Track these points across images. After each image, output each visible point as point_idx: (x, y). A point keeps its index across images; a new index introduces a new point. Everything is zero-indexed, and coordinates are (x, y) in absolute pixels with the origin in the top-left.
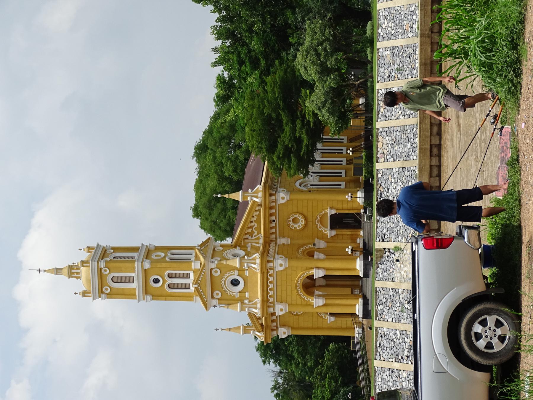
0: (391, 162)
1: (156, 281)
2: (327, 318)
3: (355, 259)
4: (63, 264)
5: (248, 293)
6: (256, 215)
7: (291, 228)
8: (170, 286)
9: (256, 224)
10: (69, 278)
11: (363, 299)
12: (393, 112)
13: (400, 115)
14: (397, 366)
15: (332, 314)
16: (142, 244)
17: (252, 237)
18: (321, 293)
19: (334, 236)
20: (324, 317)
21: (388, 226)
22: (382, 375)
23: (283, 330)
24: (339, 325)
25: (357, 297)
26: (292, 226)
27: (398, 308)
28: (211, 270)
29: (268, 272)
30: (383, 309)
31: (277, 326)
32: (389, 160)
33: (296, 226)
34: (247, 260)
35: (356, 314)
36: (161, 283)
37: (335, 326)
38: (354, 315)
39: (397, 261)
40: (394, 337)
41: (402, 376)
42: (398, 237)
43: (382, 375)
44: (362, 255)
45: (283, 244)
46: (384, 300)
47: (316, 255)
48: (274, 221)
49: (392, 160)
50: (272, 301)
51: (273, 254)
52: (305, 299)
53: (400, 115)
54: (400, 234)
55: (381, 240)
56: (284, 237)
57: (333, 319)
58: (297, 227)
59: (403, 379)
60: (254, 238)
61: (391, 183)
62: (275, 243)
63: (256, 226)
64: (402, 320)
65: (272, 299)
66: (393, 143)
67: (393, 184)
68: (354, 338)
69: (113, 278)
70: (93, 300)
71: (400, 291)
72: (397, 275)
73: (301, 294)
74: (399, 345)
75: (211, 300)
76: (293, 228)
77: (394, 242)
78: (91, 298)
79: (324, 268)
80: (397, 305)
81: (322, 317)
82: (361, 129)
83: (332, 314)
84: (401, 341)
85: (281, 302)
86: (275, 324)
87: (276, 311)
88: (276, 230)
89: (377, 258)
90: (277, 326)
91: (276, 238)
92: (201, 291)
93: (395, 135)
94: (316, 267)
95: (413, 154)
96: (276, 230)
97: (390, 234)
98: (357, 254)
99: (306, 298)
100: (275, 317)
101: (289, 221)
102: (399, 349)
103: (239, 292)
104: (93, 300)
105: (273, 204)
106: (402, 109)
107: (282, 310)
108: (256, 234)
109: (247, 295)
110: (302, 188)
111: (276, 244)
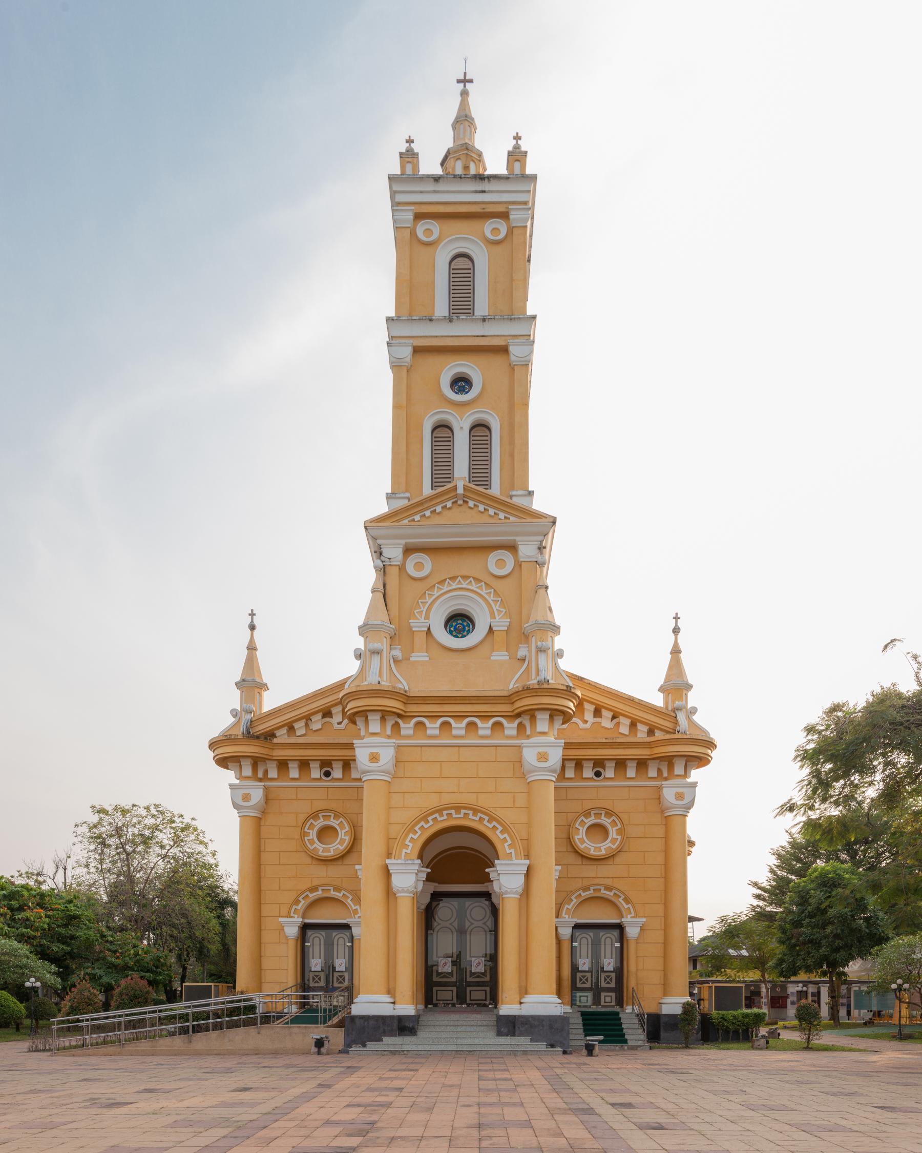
2: (292, 914)
9: (588, 726)
20: (294, 907)
28: (512, 548)
31: (265, 778)
33: (583, 831)
37: (267, 937)
48: (327, 774)
50: (403, 732)
52: (411, 835)
57: (292, 931)
63: (582, 725)
75: (403, 542)
76: (577, 826)
79: (526, 891)
82: (900, 1023)
85: (398, 762)
86: (273, 774)
89: (136, 1033)
92: (439, 509)
99: (415, 837)
101: (598, 815)
107: (374, 758)
109: (420, 656)
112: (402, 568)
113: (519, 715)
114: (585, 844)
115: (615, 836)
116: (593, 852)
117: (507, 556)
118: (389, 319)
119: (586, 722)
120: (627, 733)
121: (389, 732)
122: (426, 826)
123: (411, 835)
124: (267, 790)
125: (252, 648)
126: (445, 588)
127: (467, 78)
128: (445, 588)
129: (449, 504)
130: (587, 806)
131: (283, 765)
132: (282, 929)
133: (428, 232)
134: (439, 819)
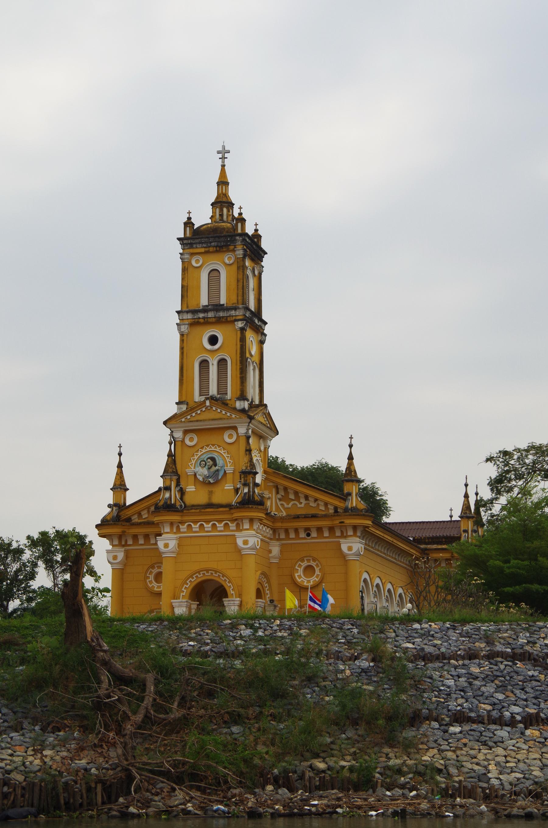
1: (213, 340)
4: (233, 194)
5: (194, 490)
6: (318, 505)
7: (296, 563)
8: (204, 364)
17: (280, 500)
26: (300, 566)
28: (235, 428)
29: (233, 520)
31: (126, 545)
33: (300, 571)
34: (275, 497)
36: (208, 347)
45: (270, 551)
48: (308, 535)
50: (181, 530)
52: (185, 586)
56: (281, 552)
58: (299, 574)
60: (279, 503)
62: (272, 537)
63: (299, 506)
65: (185, 530)
69: (216, 272)
73: (187, 584)
75: (183, 429)
76: (296, 568)
78: (182, 236)
85: (179, 545)
86: (130, 542)
88: (293, 539)
91: (279, 539)
92: (199, 412)
94: (241, 602)
96: (293, 539)
99: (187, 586)
101: (308, 561)
105: (338, 533)
107: (166, 546)
108: (286, 506)
111: (271, 539)
112: (183, 441)
113: (236, 520)
114: (311, 581)
115: (318, 573)
118: (178, 312)
119: (301, 503)
120: (324, 509)
121: (175, 531)
122: (193, 580)
123: (185, 586)
125: (120, 466)
128: (204, 451)
129: (204, 409)
131: (135, 537)
134: (199, 576)
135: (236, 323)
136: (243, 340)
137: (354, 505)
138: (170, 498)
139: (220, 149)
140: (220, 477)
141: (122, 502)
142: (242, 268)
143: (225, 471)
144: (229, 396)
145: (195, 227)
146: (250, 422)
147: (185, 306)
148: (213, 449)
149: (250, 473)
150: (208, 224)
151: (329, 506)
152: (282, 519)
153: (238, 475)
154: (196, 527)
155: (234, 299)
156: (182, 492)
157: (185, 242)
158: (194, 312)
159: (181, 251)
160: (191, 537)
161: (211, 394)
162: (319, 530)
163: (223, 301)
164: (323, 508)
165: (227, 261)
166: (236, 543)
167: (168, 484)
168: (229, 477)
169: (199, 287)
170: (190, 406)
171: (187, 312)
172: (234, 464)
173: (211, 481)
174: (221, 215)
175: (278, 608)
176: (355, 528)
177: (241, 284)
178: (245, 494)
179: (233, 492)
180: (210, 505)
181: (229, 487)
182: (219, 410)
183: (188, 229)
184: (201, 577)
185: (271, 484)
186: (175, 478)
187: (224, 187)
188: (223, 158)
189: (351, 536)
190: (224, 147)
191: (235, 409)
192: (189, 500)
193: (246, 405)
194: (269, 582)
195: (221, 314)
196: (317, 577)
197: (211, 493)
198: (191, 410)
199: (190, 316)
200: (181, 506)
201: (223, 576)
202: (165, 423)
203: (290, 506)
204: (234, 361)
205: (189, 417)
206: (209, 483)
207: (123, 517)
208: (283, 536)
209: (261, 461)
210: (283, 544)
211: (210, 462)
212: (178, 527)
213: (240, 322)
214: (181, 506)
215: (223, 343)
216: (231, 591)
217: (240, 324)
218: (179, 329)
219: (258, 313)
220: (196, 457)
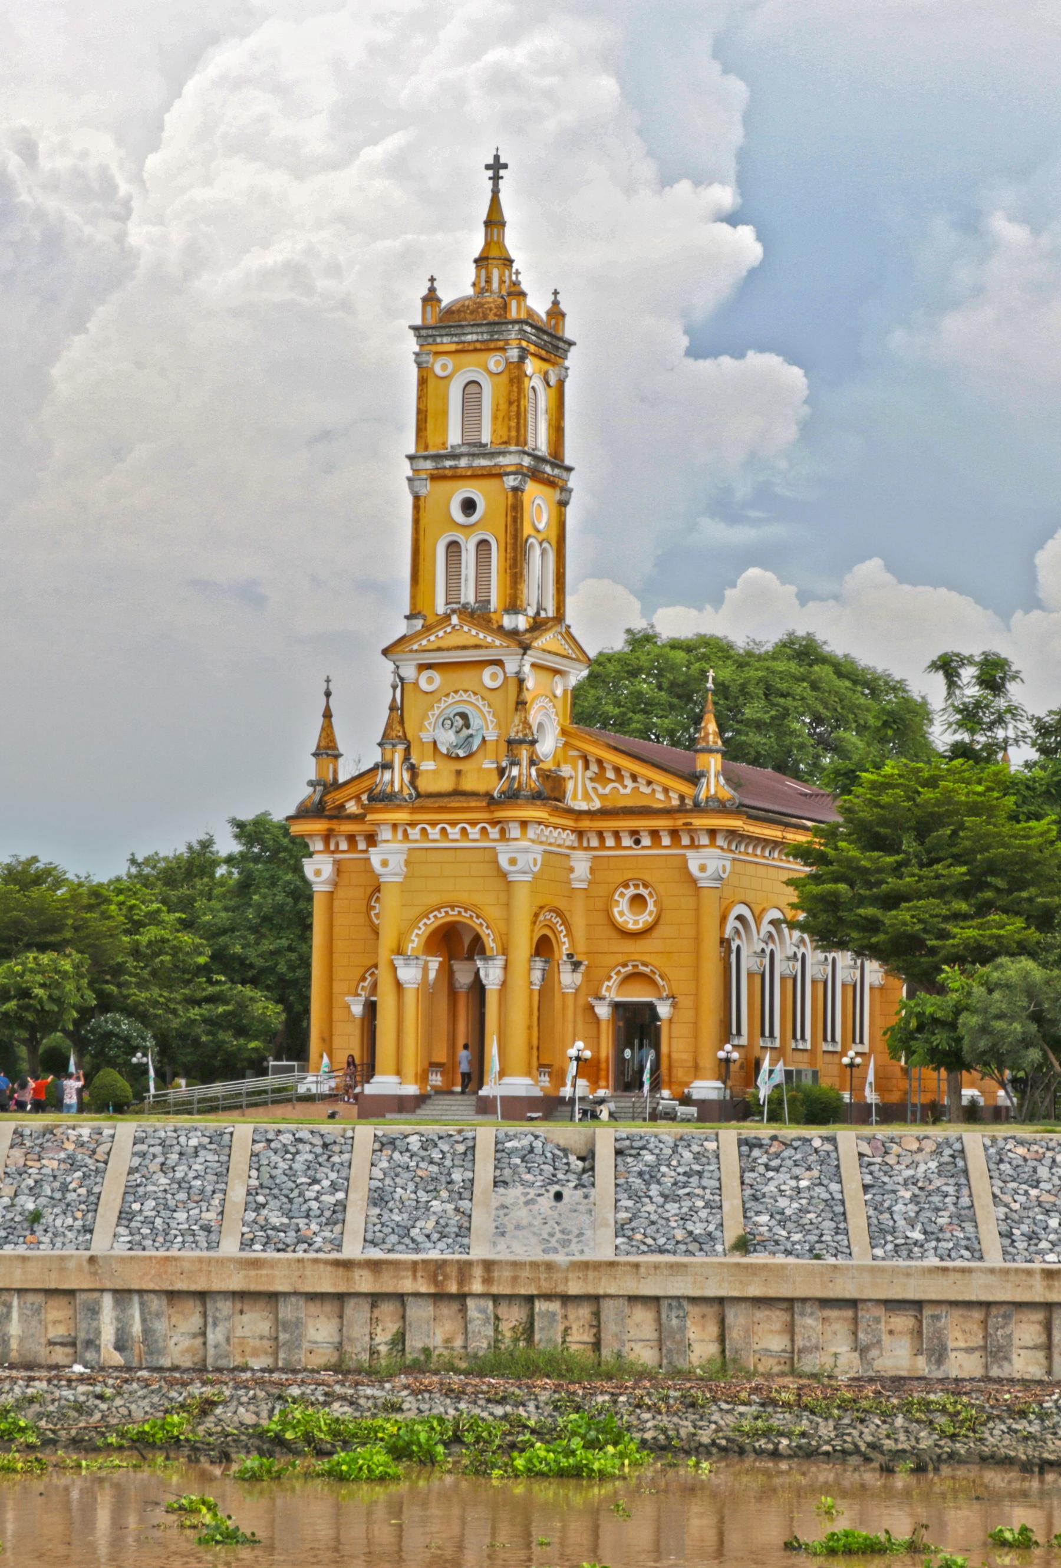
0: (859, 1176)
1: (469, 506)
3: (529, 1074)
6: (654, 790)
8: (454, 547)
10: (476, 261)
11: (416, 1097)
12: (1014, 1185)
13: (1006, 1206)
14: (237, 1193)
15: (371, 1008)
16: (569, 469)
17: (591, 779)
18: (432, 975)
19: (595, 1015)
21: (663, 1169)
22: (209, 1146)
23: (328, 870)
24: (339, 1028)
25: (422, 1078)
26: (622, 895)
27: (413, 1196)
28: (499, 663)
29: (494, 823)
30: (407, 1150)
31: (337, 850)
32: (864, 1170)
35: (372, 1076)
36: (458, 515)
38: (370, 1070)
39: (558, 1196)
40: (326, 1183)
41: (204, 1209)
42: (630, 1198)
43: (209, 1146)
44: (541, 1094)
45: (571, 870)
46: (436, 1155)
47: (539, 964)
48: (637, 842)
49: (868, 1179)
50: (411, 837)
51: (544, 839)
53: (1006, 1206)
54: (639, 1205)
55: (618, 1145)
56: (592, 870)
57: (357, 1009)
59: (197, 1211)
60: (590, 785)
61: (797, 1178)
62: (576, 844)
63: (622, 791)
64: (377, 1211)
66: (920, 1184)
67: (793, 1183)
68: (304, 1069)
70: (415, 328)
71: (464, 1204)
72: (514, 1194)
74: (301, 1199)
76: (616, 897)
77: (617, 1185)
78: (418, 322)
79: (504, 983)
80: (421, 1193)
81: (364, 979)
83: (371, 1008)
84: (314, 1205)
86: (344, 846)
87: (382, 847)
88: (610, 848)
90: (337, 850)
91: (588, 848)
92: (441, 634)
93: (945, 1188)
95: (890, 1247)
96: (610, 848)
97: (640, 1174)
98: (542, 1078)
100: (362, 846)
101: (636, 886)
102: (287, 1197)
103: (435, 743)
104: (415, 328)
105: (685, 841)
106: (1024, 1214)
107: (385, 863)
108: (601, 791)
110: (731, 923)
111: (574, 848)
112: (416, 684)
116: (631, 926)
117: (496, 669)
118: (411, 458)
121: (400, 835)
124: (337, 863)
125: (328, 715)
126: (450, 700)
127: (502, 161)
129: (449, 629)
130: (628, 875)
132: (349, 1007)
133: (444, 367)
135: (505, 478)
136: (516, 510)
137: (712, 792)
138: (392, 782)
139: (491, 161)
140: (475, 748)
141: (331, 777)
142: (516, 377)
143: (484, 739)
144: (494, 604)
145: (443, 304)
146: (524, 654)
147: (422, 446)
148: (465, 697)
149: (521, 742)
150: (469, 298)
151: (671, 794)
152: (590, 814)
153: (504, 746)
154: (434, 832)
155: (503, 433)
156: (413, 770)
157: (424, 332)
158: (437, 457)
159: (417, 349)
160: (427, 849)
161: (463, 601)
162: (655, 834)
163: (486, 438)
164: (660, 796)
165: (492, 366)
166: (497, 862)
167: (388, 757)
168: (490, 748)
169: (445, 413)
170: (429, 622)
171: (425, 458)
172: (499, 725)
173: (461, 753)
174: (488, 281)
175: (582, 968)
176: (712, 833)
177: (514, 408)
178: (514, 778)
179: (495, 775)
180: (457, 793)
181: (489, 765)
182: (474, 632)
183: (429, 308)
184: (453, 915)
185: (575, 753)
186: (401, 747)
187: (495, 231)
188: (496, 179)
189: (705, 846)
190: (497, 158)
191: (501, 627)
192: (425, 785)
193: (522, 622)
194: (565, 923)
195: (484, 462)
196: (636, 922)
197: (459, 773)
198: (427, 629)
199: (429, 465)
200: (410, 795)
201: (478, 917)
202: (385, 652)
203: (607, 790)
204: (502, 545)
205: (424, 642)
206: (458, 758)
207: (330, 805)
208: (595, 842)
209: (557, 714)
210: (595, 857)
211: (459, 722)
212: (405, 833)
213: (512, 477)
214: (410, 795)
215: (485, 513)
216: (491, 943)
217: (511, 481)
218: (411, 488)
219: (556, 457)
220: (437, 712)
